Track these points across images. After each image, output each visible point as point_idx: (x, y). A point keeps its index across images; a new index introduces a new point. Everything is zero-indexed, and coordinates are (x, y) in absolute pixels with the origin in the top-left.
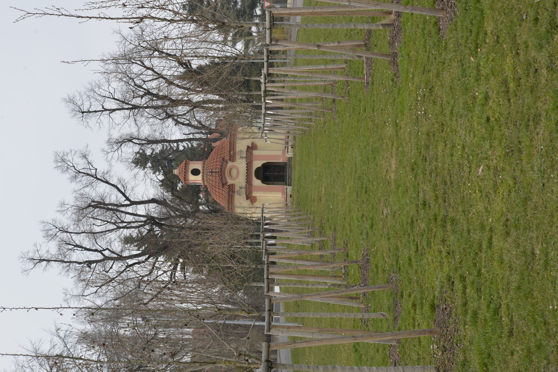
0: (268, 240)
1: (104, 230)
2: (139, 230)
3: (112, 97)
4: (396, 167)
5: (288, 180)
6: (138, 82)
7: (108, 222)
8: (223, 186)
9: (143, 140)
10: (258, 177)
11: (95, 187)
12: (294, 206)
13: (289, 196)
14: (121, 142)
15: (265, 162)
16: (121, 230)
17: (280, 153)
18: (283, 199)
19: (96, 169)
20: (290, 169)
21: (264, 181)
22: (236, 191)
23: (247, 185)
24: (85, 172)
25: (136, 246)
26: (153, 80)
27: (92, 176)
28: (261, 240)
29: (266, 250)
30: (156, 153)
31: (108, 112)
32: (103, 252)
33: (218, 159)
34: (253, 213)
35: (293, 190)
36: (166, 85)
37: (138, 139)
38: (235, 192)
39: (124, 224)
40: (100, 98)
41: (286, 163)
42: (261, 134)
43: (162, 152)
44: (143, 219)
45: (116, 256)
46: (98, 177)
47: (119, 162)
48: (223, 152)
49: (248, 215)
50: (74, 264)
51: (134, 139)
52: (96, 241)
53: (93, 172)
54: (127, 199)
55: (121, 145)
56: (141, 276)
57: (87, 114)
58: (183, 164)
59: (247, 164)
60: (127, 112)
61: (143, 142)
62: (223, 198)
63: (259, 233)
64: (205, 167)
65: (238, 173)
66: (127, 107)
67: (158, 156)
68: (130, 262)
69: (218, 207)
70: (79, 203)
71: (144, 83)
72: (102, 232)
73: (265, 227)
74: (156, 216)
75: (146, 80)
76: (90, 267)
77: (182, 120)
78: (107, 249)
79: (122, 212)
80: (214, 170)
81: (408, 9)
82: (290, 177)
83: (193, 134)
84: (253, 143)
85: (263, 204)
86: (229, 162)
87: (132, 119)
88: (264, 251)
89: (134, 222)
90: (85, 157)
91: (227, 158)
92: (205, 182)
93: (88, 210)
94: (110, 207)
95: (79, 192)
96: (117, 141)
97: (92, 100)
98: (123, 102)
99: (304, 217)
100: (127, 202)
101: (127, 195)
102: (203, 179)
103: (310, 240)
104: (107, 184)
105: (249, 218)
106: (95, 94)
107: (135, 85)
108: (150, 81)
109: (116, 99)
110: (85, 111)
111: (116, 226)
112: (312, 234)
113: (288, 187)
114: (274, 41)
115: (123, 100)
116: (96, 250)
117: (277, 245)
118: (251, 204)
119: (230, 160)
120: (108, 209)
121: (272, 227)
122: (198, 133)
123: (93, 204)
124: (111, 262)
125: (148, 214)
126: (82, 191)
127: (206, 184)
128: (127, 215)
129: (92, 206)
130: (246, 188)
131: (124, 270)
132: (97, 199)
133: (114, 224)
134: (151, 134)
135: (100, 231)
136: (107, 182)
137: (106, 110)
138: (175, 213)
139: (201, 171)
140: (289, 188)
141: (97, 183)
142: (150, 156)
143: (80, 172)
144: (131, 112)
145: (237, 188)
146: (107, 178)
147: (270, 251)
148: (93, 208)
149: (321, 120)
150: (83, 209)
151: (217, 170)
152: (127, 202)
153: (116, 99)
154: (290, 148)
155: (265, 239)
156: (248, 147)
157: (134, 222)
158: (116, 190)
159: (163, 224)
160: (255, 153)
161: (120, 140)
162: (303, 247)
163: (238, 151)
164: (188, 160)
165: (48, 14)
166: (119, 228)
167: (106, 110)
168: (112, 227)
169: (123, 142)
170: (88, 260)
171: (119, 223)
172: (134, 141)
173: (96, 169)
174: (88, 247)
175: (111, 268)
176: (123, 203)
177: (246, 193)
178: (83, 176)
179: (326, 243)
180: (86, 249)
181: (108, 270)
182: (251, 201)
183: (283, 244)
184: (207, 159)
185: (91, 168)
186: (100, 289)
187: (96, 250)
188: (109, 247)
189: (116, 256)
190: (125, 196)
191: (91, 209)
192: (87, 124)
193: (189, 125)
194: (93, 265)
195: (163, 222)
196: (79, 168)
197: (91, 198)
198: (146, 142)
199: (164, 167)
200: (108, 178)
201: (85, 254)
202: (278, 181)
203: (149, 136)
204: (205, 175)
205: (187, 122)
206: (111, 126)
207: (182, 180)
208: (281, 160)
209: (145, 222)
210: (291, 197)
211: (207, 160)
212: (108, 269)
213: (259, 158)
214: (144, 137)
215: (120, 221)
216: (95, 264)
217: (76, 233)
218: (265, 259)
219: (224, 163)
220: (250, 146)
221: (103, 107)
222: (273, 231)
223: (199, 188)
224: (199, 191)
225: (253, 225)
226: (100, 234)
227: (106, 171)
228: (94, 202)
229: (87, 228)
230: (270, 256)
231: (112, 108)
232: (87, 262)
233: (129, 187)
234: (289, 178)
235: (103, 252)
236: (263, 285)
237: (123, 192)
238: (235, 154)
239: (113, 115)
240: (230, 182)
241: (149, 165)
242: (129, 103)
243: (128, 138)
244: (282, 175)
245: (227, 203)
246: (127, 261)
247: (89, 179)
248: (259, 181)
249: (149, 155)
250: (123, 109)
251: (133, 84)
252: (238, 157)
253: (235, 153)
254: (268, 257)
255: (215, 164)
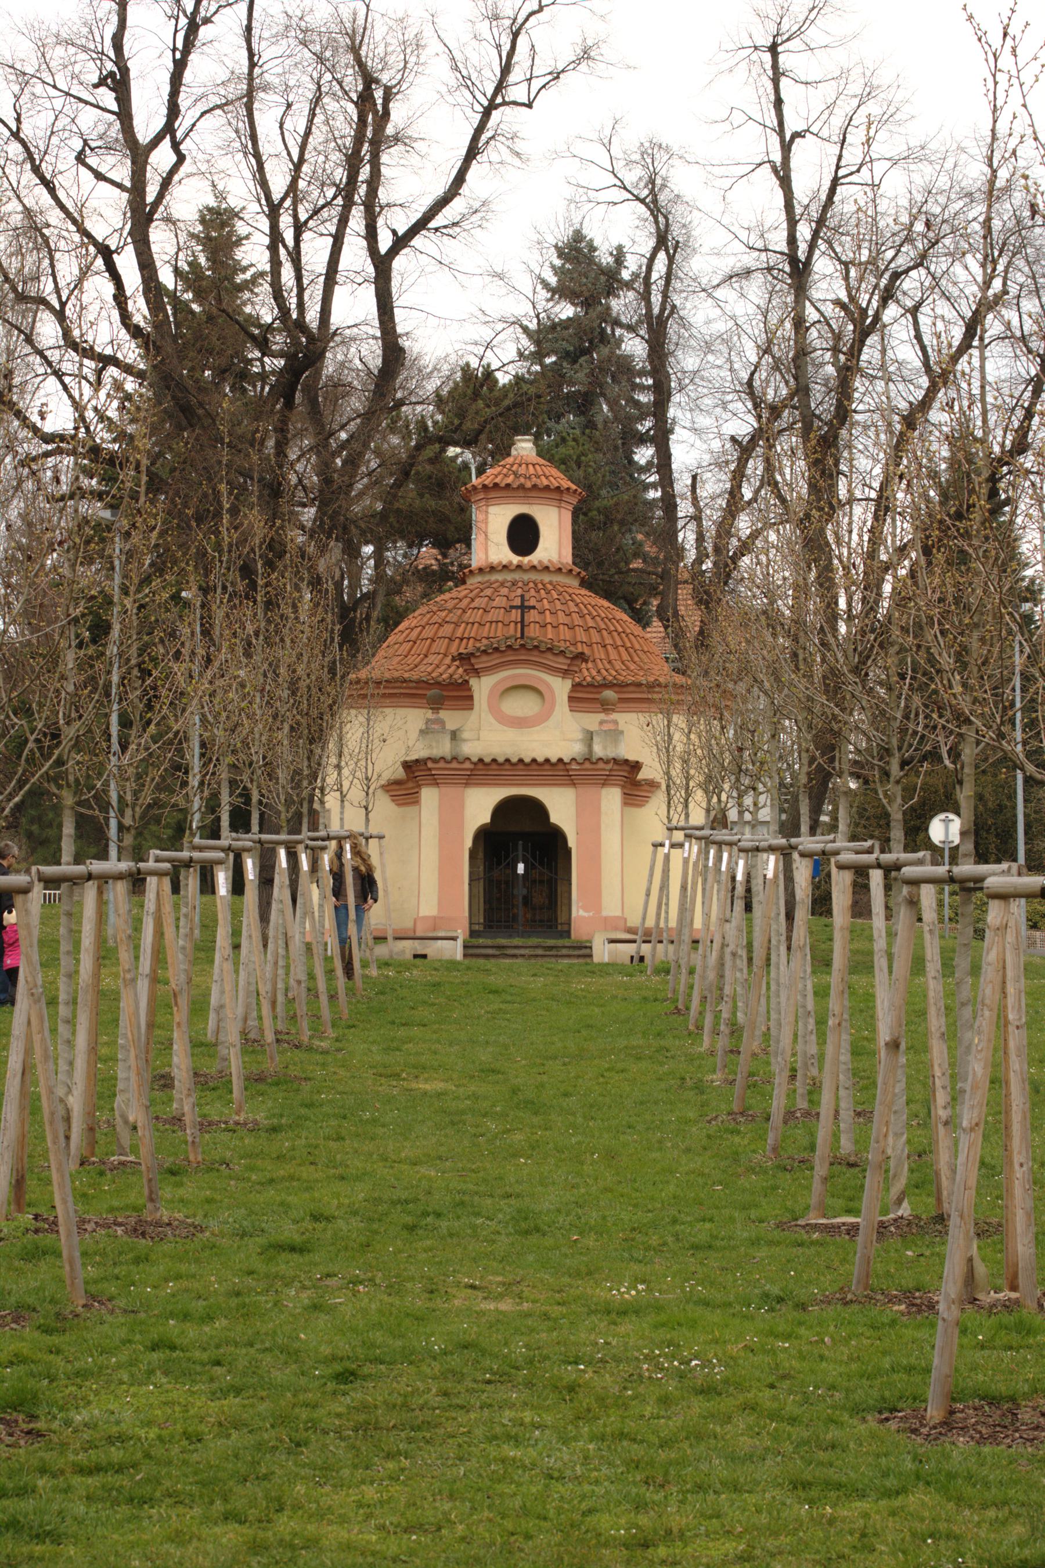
0: (226, 870)
1: (265, 148)
2: (262, 274)
3: (841, 173)
4: (482, 1313)
5: (489, 942)
6: (911, 284)
7: (298, 167)
8: (464, 658)
9: (665, 296)
10: (504, 809)
11: (450, 99)
12: (374, 972)
13: (419, 947)
14: (655, 201)
15: (572, 842)
16: (265, 224)
17: (611, 907)
18: (410, 924)
19: (529, 105)
20: (540, 952)
21: (483, 835)
22: (443, 714)
23: (467, 765)
24: (515, 59)
25: (194, 264)
26: (923, 348)
27: (500, 88)
28: (227, 838)
29: (188, 864)
30: (620, 341)
31: (777, 157)
32: (167, 142)
33: (581, 636)
34: (343, 797)
35: (451, 965)
36: (903, 405)
37: (668, 277)
38: (436, 710)
39: (289, 236)
40: (838, 121)
41: (568, 934)
42: (682, 824)
43: (624, 367)
44: (312, 316)
45: (150, 198)
46: (496, 115)
47: (569, 191)
48: (613, 655)
49: (331, 779)
50: (115, 19)
51: (671, 259)
52: (218, 107)
53: (517, 92)
54: (401, 242)
55: (642, 201)
56: (63, 305)
57: (768, 65)
58: (557, 478)
59: (560, 760)
60: (779, 241)
61: (656, 299)
62: (410, 660)
63: (255, 827)
64: (546, 578)
65: (520, 723)
66: (804, 231)
67: (605, 351)
68: (127, 263)
69: (367, 640)
70: (379, 31)
71: (907, 311)
72: (254, 137)
73: (282, 853)
74: (329, 368)
75: (921, 319)
76: (101, 82)
77: (755, 467)
78: (181, 158)
79: (343, 221)
80: (532, 616)
81: (949, 1308)
82: (502, 952)
83: (697, 518)
84: (652, 785)
85: (381, 837)
86: (568, 684)
87: (750, 260)
88: (185, 854)
89: (299, 278)
90: (586, 55)
91: (587, 672)
92: (479, 579)
93: (350, 71)
94: (365, 173)
95: (428, 32)
96: (659, 181)
97: (828, 91)
98: (821, 222)
99: (326, 1012)
100: (385, 242)
101: (417, 241)
102: (492, 569)
103: (232, 1035)
104: (463, 152)
105: (319, 783)
106: (855, 102)
107: (896, 276)
108: (918, 337)
109: (832, 191)
110: (782, 58)
111: (283, 200)
112: (250, 1043)
113: (460, 942)
114: (909, 893)
115: (831, 223)
116: (173, 111)
117: (207, 898)
118: (383, 782)
119: (576, 687)
120: (353, 163)
121: (280, 890)
122: (700, 538)
123: (378, 94)
124: (123, 173)
125: (335, 334)
126: (433, 45)
127: (473, 581)
128: (330, 240)
129: (367, 87)
130: (455, 758)
131: (89, 235)
132: (398, 113)
133: (293, 187)
134: (694, 331)
135: (259, 130)
136: (472, 153)
137: (786, 148)
138: (343, 445)
139: (526, 560)
140: (455, 950)
141: (469, 111)
142: (606, 315)
143: (516, 35)
144: (774, 259)
145: (451, 718)
146: (491, 154)
147: (187, 878)
148: (360, 96)
149: (714, 1071)
150: (355, 50)
151: (533, 631)
152: (385, 242)
153: (832, 191)
154: (630, 949)
155: (231, 856)
156: (636, 766)
157: (299, 278)
158: (439, 189)
159: (289, 404)
160: (612, 797)
161: (662, 198)
162: (199, 1007)
163: (616, 722)
164: (574, 501)
165: (995, 122)
166: (273, 212)
167: (786, 148)
168: (278, 185)
169: (654, 207)
170: (133, 74)
171: (295, 216)
172: (662, 256)
173: (529, 105)
174: (188, 76)
175: (99, 176)
176: (380, 222)
177: (435, 761)
178: (498, 47)
179: (220, 1097)
180: (180, 67)
181: (88, 161)
182: (398, 783)
183: (209, 925)
184: (584, 583)
185: (536, 84)
186: (7, 133)
187: (173, 111)
188: (186, 168)
189: (150, 198)
190: (415, 230)
191: (354, 84)
192: (725, 66)
193: (734, 504)
194: (108, 98)
195: (298, 397)
196: (536, 31)
197: (404, 86)
198: (656, 311)
199: (555, 377)
200: (495, 157)
201: (160, 61)
202: (488, 901)
203: (684, 323)
204: (509, 577)
205: (747, 493)
206: (716, 170)
207: (491, 475)
208: (579, 912)
209: (301, 325)
210: (416, 956)
211: (576, 583)
212: (92, 161)
213: (589, 816)
214: (677, 303)
215: (303, 216)
216: (115, 107)
217: (249, 29)
218: (155, 859)
219: (562, 663)
220: (641, 776)
221: (796, 135)
222: (266, 881)
223: (459, 541)
224: (443, 544)
225: (289, 802)
226: (243, 126)
227: (519, 146)
228: (387, 99)
229: (271, 72)
230: (167, 882)
231: (794, 176)
232: (125, 71)
233: (450, 248)
234: (499, 947)
235: (167, 142)
236: (64, 859)
237: (432, 224)
238: (606, 711)
239: (767, 179)
240: (482, 687)
241: (566, 311)
242: (822, 246)
243: (676, 231)
244: (515, 918)
245: (387, 675)
246: (130, 249)
247: (487, 73)
248: (485, 818)
249: (609, 308)
250: (792, 223)
251: (902, 262)
252: (592, 720)
253: (606, 707)
254: (160, 874)
255: (562, 618)
